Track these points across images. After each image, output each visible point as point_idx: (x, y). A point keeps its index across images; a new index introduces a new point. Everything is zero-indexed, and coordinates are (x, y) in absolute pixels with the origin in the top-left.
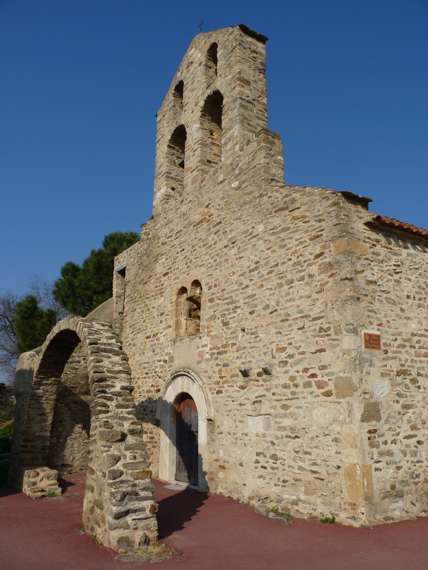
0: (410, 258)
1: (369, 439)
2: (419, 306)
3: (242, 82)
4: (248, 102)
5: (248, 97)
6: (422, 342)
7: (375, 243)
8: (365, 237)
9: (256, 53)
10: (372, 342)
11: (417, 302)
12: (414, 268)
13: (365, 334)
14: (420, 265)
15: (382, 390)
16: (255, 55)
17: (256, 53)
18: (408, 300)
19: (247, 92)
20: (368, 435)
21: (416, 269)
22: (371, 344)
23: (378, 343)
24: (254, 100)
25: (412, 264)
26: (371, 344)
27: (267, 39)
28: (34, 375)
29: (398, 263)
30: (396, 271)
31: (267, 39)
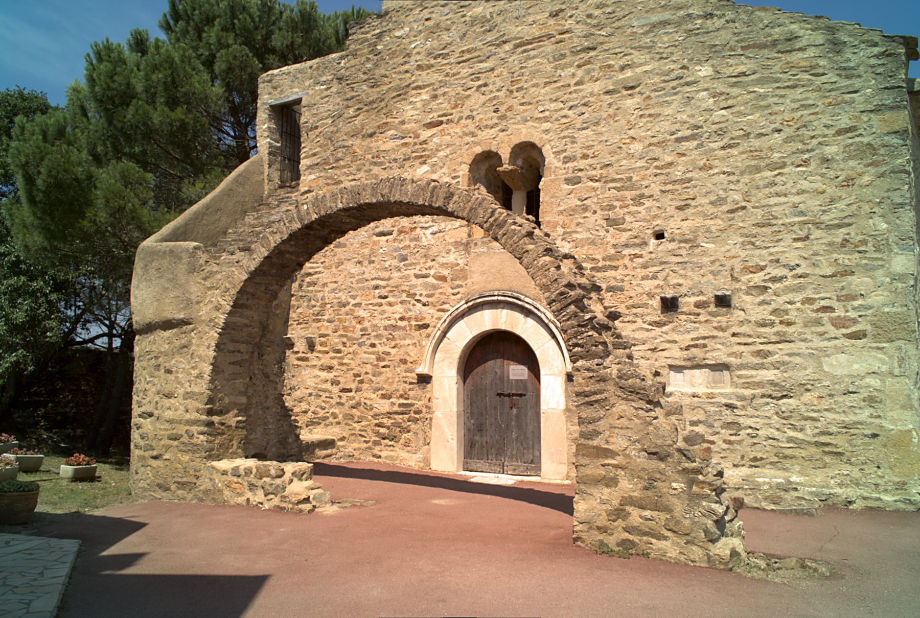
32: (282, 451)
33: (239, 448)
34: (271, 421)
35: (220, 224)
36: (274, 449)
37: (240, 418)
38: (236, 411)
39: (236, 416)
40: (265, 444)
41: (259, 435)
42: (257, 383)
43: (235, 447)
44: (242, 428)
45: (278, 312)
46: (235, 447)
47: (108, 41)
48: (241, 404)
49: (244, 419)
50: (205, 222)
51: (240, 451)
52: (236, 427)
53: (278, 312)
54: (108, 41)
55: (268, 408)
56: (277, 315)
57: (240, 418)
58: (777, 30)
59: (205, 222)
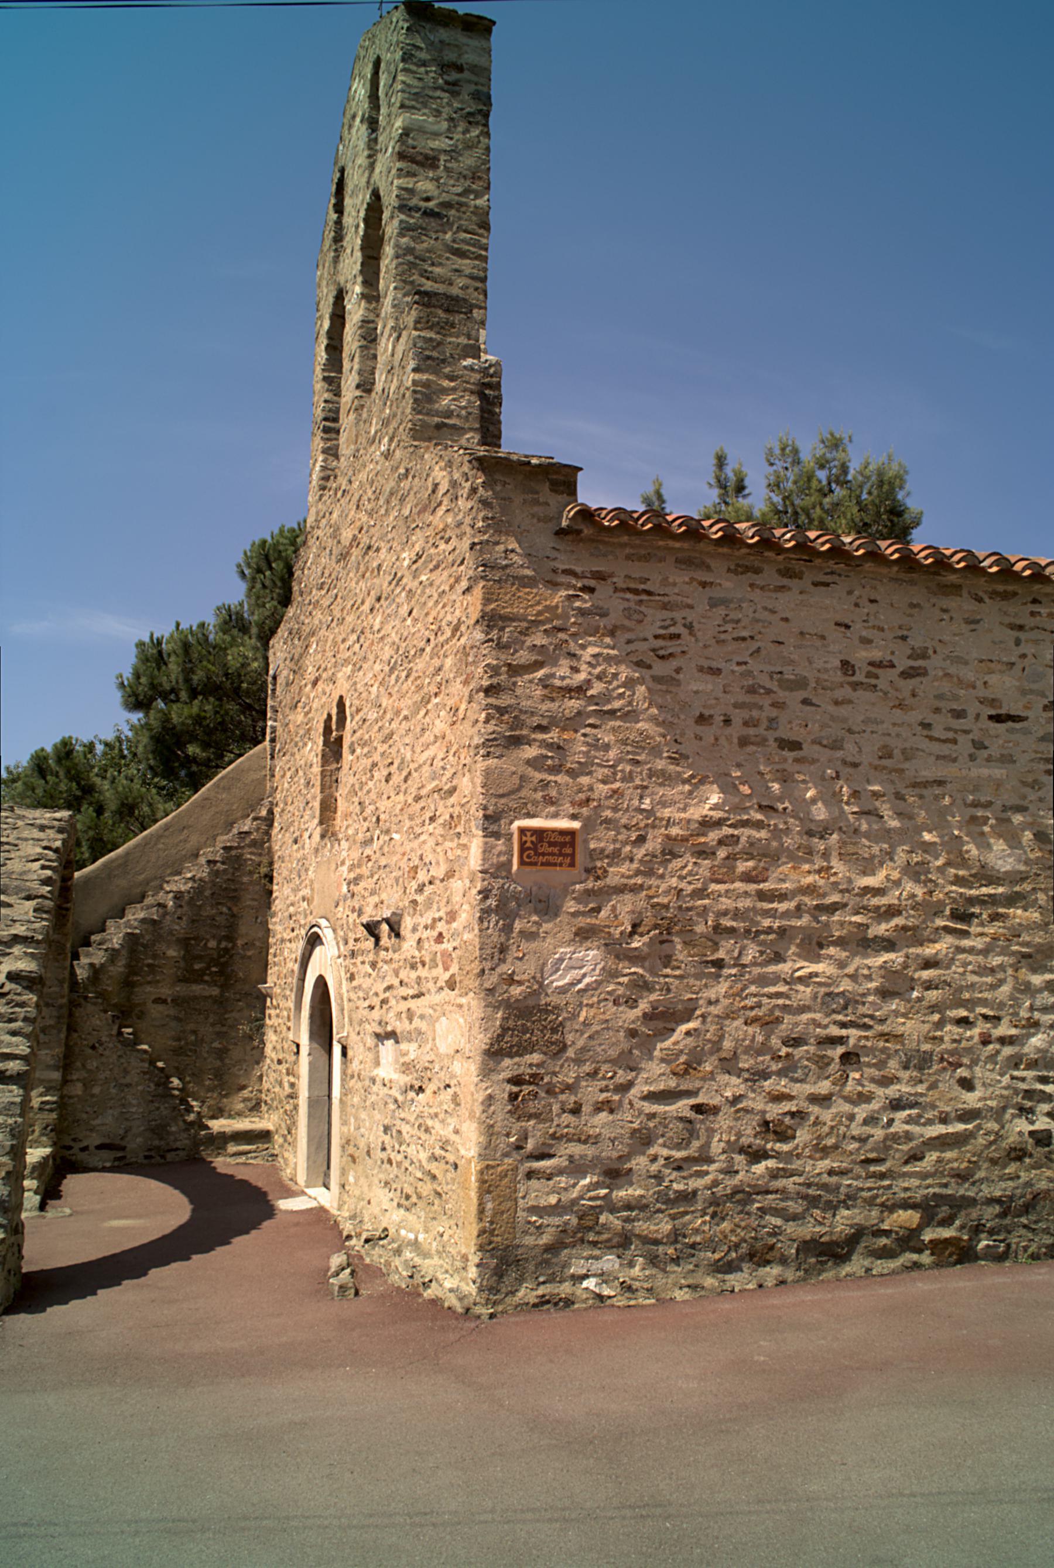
0: (721, 611)
1: (513, 1097)
2: (743, 742)
3: (413, 161)
4: (428, 213)
5: (428, 199)
6: (743, 839)
7: (592, 583)
8: (554, 571)
9: (460, 69)
10: (545, 848)
11: (736, 730)
12: (736, 639)
13: (522, 831)
14: (758, 627)
15: (575, 974)
16: (454, 76)
17: (460, 69)
18: (700, 729)
19: (425, 185)
20: (509, 1087)
21: (744, 639)
22: (543, 854)
23: (568, 851)
24: (447, 205)
25: (729, 627)
26: (543, 854)
27: (494, 23)
28: (919, 950)
29: (672, 630)
30: (661, 653)
31: (494, 23)
32: (156, 1143)
33: (43, 1135)
34: (134, 1102)
35: (188, 846)
36: (139, 1140)
37: (48, 1098)
38: (41, 1089)
39: (41, 1095)
40: (121, 1132)
41: (109, 1120)
42: (107, 1053)
43: (37, 1133)
44: (51, 1110)
45: (249, 953)
46: (37, 1133)
47: (832, 435)
48: (50, 1081)
49: (55, 1099)
50: (161, 846)
51: (44, 1139)
52: (40, 1109)
53: (249, 953)
54: (832, 435)
55: (128, 1085)
56: (250, 957)
57: (48, 1098)
58: (430, 283)
59: (161, 846)
